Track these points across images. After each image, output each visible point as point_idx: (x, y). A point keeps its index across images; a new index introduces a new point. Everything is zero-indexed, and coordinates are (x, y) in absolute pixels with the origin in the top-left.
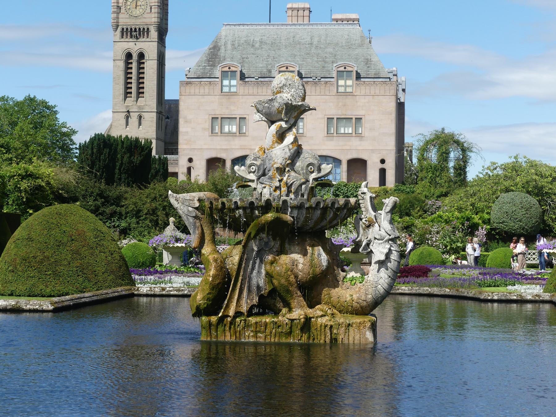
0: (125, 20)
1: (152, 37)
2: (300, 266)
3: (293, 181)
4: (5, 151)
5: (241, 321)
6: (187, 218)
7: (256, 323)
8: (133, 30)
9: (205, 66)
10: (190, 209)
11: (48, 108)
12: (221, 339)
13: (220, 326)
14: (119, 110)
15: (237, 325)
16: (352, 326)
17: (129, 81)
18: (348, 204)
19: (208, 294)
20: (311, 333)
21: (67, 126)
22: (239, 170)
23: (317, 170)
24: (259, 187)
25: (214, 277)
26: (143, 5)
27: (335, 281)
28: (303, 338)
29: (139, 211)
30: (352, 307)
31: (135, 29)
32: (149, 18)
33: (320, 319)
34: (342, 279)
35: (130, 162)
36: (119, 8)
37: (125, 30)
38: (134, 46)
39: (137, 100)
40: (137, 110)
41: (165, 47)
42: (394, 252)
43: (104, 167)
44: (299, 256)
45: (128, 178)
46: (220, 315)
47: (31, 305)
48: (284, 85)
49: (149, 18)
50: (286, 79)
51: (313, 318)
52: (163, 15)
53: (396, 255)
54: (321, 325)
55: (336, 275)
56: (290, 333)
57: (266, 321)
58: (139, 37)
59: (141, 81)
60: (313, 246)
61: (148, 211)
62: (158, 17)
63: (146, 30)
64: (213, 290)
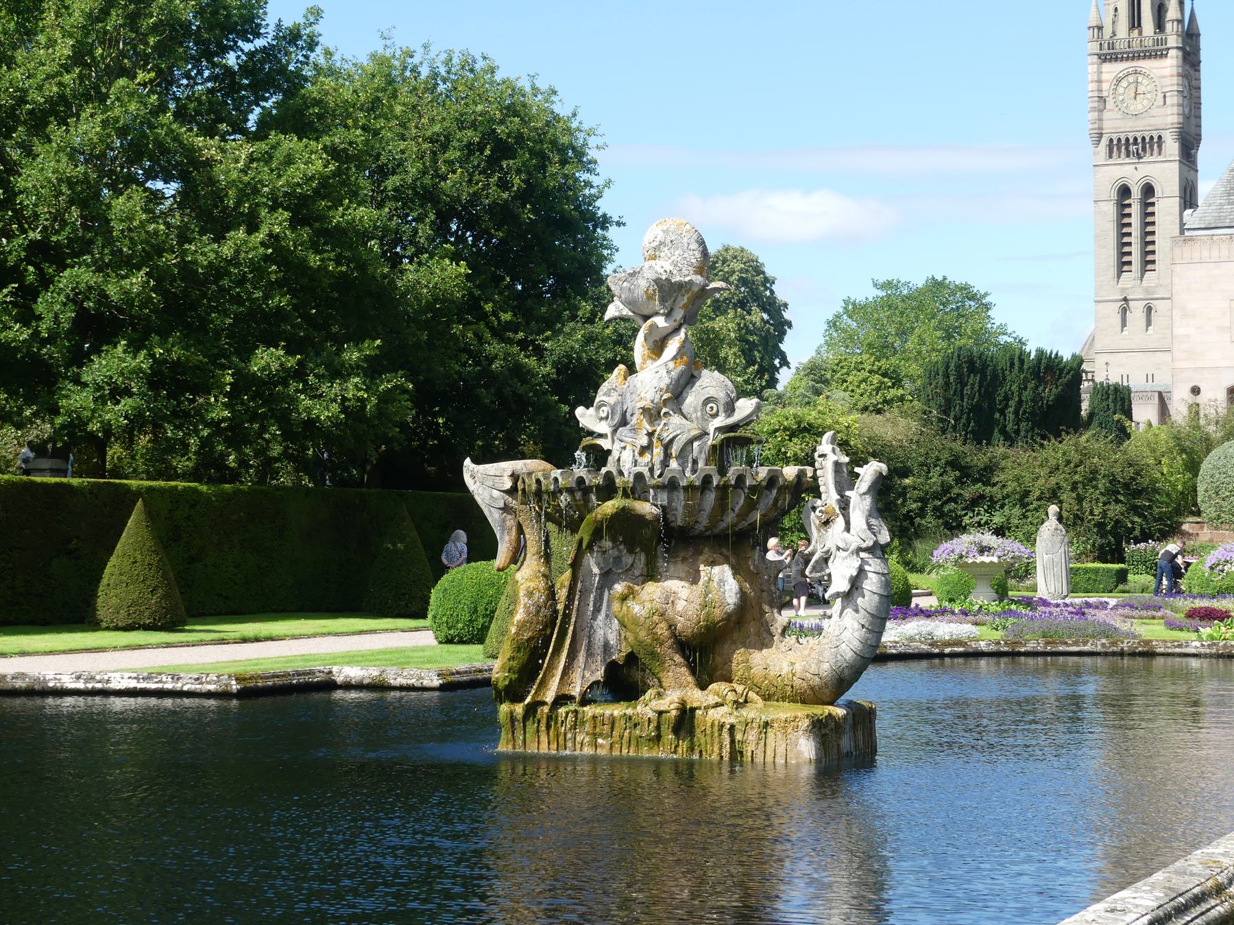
0: (1116, 124)
1: (1169, 152)
2: (680, 605)
3: (674, 434)
4: (890, 384)
5: (567, 713)
6: (490, 512)
7: (594, 717)
8: (1131, 141)
9: (1220, 204)
10: (496, 493)
11: (973, 297)
12: (532, 749)
13: (529, 723)
14: (1107, 298)
15: (560, 722)
16: (772, 727)
17: (1126, 240)
18: (778, 477)
19: (509, 660)
20: (695, 739)
21: (1009, 331)
22: (583, 415)
23: (725, 412)
24: (617, 447)
25: (522, 626)
26: (1149, 92)
27: (765, 635)
28: (680, 750)
29: (1027, 493)
30: (792, 687)
31: (1136, 139)
32: (1161, 116)
33: (713, 710)
34: (780, 631)
35: (1036, 398)
36: (1102, 99)
37: (1115, 142)
38: (1133, 173)
39: (1142, 277)
40: (1142, 297)
41: (1197, 171)
42: (870, 575)
43: (970, 410)
44: (683, 583)
45: (1032, 429)
46: (528, 700)
47: (404, 677)
48: (661, 243)
49: (1161, 116)
50: (666, 232)
51: (699, 708)
52: (1190, 110)
53: (875, 581)
54: (712, 725)
55: (767, 622)
56: (658, 738)
57: (612, 715)
58: (1142, 154)
59: (1149, 238)
60: (713, 564)
61: (1042, 493)
62: (1178, 114)
63: (1156, 140)
64: (519, 651)
